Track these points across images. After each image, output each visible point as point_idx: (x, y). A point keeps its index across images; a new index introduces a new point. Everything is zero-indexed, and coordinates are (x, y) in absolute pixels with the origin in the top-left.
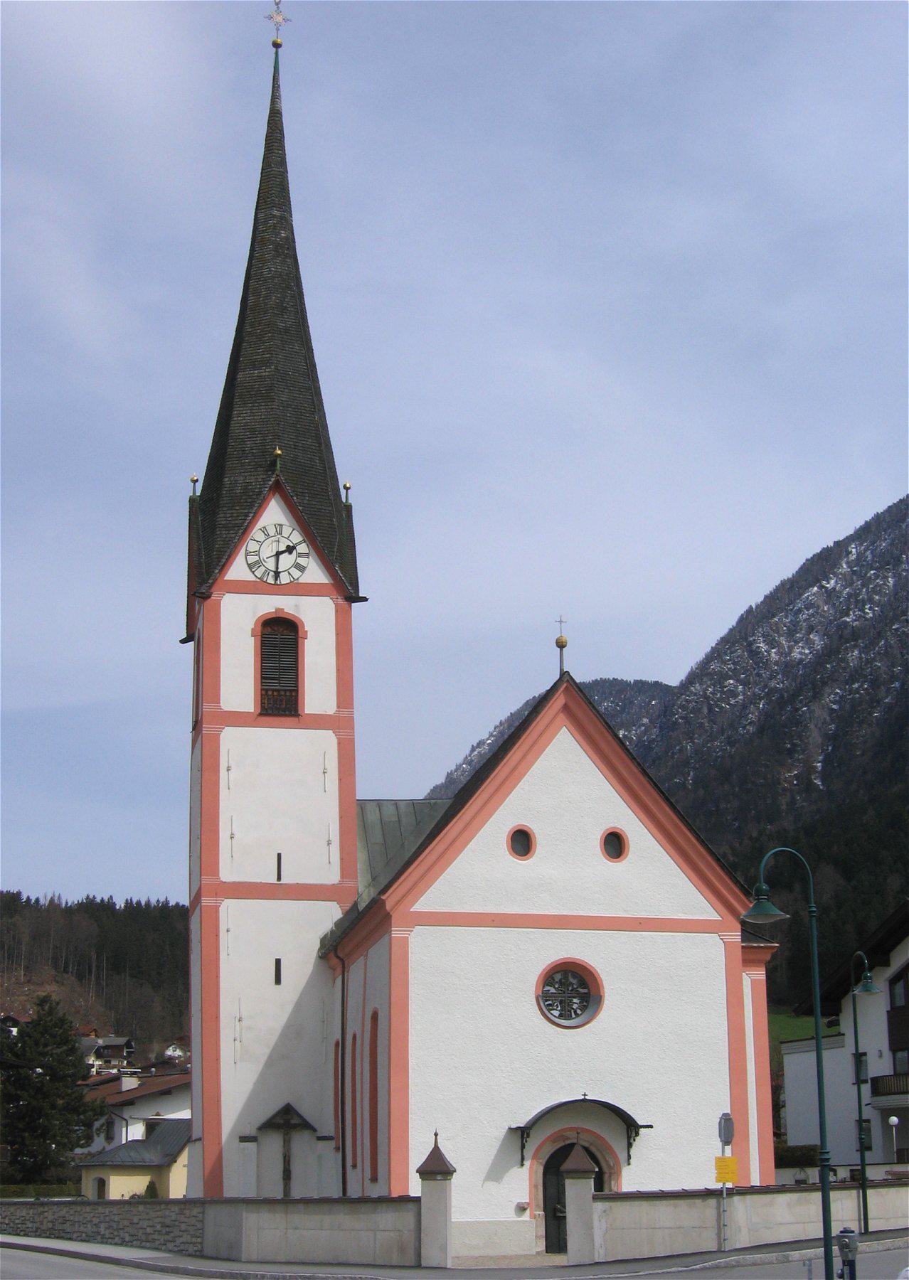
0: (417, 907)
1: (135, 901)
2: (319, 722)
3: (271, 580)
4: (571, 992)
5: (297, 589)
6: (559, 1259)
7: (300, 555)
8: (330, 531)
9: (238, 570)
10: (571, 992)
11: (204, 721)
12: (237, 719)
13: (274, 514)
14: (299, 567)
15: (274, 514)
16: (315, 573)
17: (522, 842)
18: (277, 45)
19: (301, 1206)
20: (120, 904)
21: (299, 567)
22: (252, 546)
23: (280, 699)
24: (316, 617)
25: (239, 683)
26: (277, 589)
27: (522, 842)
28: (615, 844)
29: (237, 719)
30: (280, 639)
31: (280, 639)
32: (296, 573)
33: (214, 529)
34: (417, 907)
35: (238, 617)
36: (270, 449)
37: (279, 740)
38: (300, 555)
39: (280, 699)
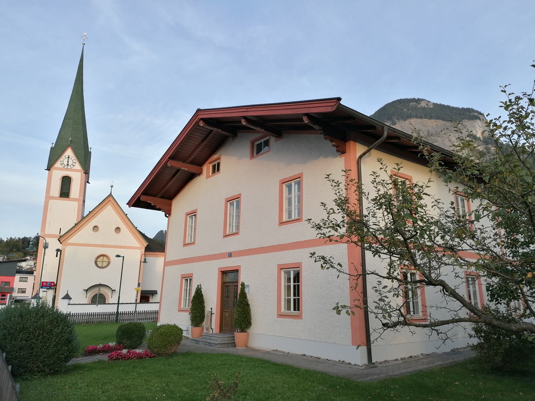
1: (9, 238)
2: (74, 200)
3: (66, 167)
4: (102, 261)
6: (228, 263)
7: (65, 166)
8: (85, 158)
9: (58, 165)
11: (48, 197)
12: (53, 198)
13: (69, 152)
14: (74, 166)
15: (69, 152)
16: (78, 166)
20: (5, 240)
22: (62, 160)
23: (65, 193)
24: (77, 177)
25: (56, 189)
28: (118, 229)
29: (53, 198)
30: (66, 181)
31: (66, 181)
32: (72, 166)
33: (55, 155)
35: (58, 175)
36: (74, 137)
37: (64, 202)
38: (65, 166)
39: (65, 193)
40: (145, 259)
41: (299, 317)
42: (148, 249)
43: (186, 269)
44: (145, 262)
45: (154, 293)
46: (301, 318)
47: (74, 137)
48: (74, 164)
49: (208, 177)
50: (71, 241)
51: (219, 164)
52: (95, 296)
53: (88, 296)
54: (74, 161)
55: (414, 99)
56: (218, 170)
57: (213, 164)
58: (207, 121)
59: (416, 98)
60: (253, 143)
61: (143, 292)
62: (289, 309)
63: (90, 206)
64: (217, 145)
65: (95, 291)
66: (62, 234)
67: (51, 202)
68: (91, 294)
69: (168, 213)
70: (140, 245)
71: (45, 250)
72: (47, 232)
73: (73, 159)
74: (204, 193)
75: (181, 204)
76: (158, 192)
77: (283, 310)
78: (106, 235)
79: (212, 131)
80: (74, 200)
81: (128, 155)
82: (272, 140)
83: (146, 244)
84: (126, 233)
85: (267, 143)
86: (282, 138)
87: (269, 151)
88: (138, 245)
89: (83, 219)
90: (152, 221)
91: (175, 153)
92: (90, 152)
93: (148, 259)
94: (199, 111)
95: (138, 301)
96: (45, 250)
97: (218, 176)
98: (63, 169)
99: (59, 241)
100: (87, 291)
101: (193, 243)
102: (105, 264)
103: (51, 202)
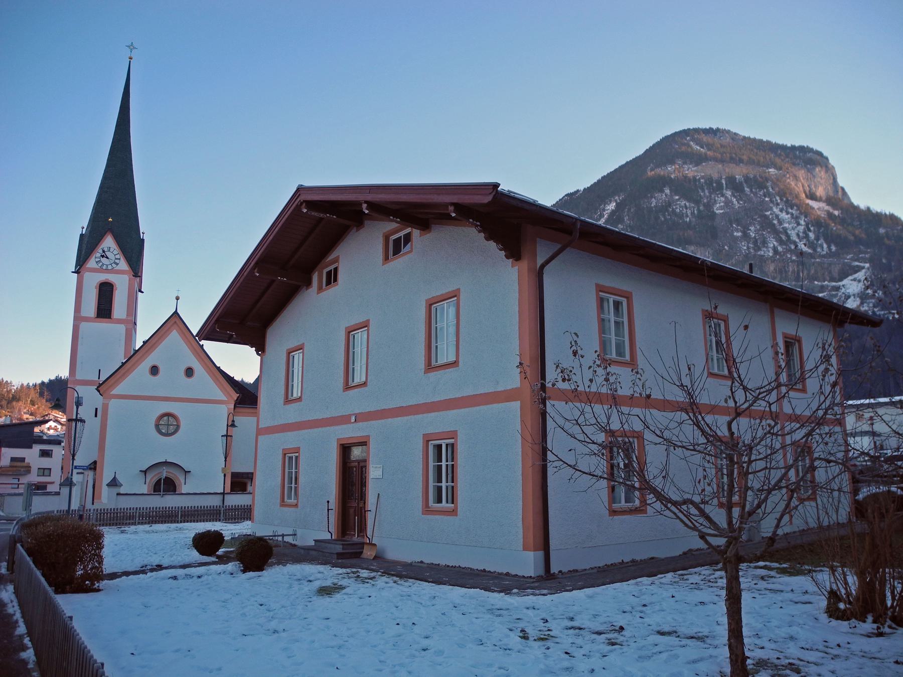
0: (113, 392)
1: (25, 384)
2: (119, 321)
4: (167, 424)
5: (113, 271)
8: (133, 250)
9: (92, 263)
10: (167, 424)
11: (78, 319)
12: (87, 319)
13: (109, 242)
14: (117, 264)
15: (109, 242)
16: (123, 265)
17: (154, 370)
18: (131, 58)
19: (539, 463)
21: (117, 264)
23: (104, 310)
26: (107, 271)
27: (154, 370)
28: (189, 372)
29: (87, 319)
30: (106, 291)
31: (106, 291)
32: (114, 265)
33: (88, 246)
34: (113, 392)
35: (93, 280)
36: (115, 219)
37: (103, 326)
39: (104, 310)
40: (233, 421)
41: (454, 512)
42: (239, 403)
43: (290, 440)
44: (233, 425)
45: (250, 476)
46: (427, 510)
47: (115, 219)
48: (117, 261)
49: (320, 289)
50: (115, 392)
51: (336, 269)
52: (158, 483)
53: (148, 481)
54: (118, 256)
55: (711, 129)
56: (335, 280)
57: (328, 269)
58: (310, 204)
59: (714, 127)
60: (387, 238)
61: (234, 475)
62: (439, 500)
63: (142, 334)
64: (333, 238)
65: (164, 473)
66: (103, 378)
67: (84, 325)
68: (152, 477)
69: (260, 349)
70: (226, 397)
71: (77, 408)
72: (79, 376)
73: (116, 252)
74: (315, 318)
75: (281, 336)
76: (247, 313)
77: (431, 503)
78: (171, 381)
79: (322, 219)
80: (119, 321)
81: (192, 265)
82: (416, 233)
83: (235, 396)
84: (203, 380)
85: (408, 238)
86: (430, 231)
87: (411, 251)
88: (223, 397)
89: (133, 357)
90: (240, 361)
91: (106, 425)
92: (143, 240)
93: (239, 420)
94: (300, 190)
95: (228, 490)
96: (77, 408)
97: (333, 291)
98: (101, 270)
99: (99, 391)
100: (145, 472)
101: (455, 364)
102: (172, 429)
103: (84, 325)
